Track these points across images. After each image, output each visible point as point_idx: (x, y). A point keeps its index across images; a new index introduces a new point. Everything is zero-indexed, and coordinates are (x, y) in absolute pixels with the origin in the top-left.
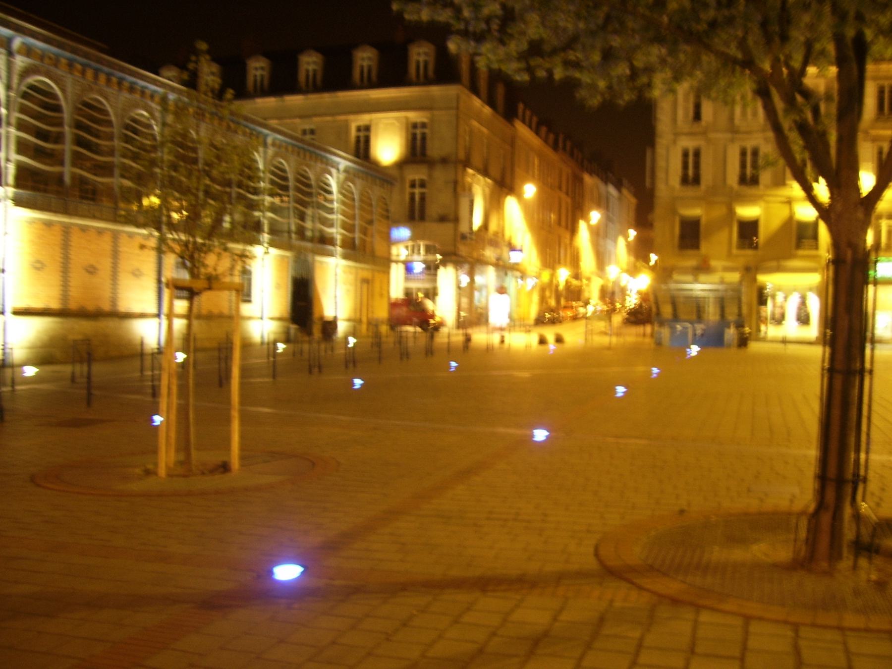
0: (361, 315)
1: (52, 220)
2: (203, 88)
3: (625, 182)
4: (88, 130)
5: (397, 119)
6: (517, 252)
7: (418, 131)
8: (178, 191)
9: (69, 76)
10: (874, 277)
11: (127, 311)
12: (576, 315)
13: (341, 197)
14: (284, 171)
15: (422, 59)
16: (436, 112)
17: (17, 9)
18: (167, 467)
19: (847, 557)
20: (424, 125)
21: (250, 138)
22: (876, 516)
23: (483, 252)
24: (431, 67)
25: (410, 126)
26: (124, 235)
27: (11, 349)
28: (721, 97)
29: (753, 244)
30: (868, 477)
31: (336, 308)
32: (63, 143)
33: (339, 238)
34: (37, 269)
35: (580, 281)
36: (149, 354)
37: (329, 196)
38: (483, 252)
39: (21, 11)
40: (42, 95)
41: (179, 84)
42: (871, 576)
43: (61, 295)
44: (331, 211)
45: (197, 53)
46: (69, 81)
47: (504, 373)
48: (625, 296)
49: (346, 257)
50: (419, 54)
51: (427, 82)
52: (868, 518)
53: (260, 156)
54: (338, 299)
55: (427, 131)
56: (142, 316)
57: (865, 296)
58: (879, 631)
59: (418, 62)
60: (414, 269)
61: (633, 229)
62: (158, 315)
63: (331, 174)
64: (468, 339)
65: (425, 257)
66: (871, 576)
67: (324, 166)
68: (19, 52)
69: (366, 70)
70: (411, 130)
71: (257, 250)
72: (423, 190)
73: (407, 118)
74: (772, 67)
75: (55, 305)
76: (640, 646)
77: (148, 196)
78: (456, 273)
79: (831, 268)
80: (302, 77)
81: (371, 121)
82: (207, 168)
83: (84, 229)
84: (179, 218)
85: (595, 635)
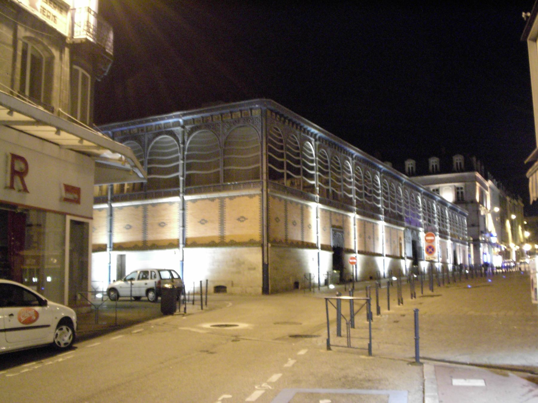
0: (123, 297)
2: (462, 237)
3: (519, 197)
4: (274, 152)
5: (450, 186)
6: (489, 225)
7: (460, 191)
8: (167, 110)
9: (302, 191)
11: (60, 319)
13: (404, 197)
14: (325, 157)
15: (410, 166)
16: (467, 183)
17: (43, 82)
19: (350, 292)
20: (462, 188)
22: (186, 242)
23: (155, 288)
24: (463, 164)
25: (456, 188)
27: (314, 291)
30: (412, 357)
31: (319, 272)
33: (449, 233)
34: (127, 229)
37: (349, 175)
38: (155, 288)
41: (70, 115)
42: (183, 162)
43: (255, 240)
44: (378, 195)
46: (329, 150)
47: (160, 145)
48: (329, 346)
49: (386, 220)
50: (457, 160)
51: (462, 171)
53: (378, 177)
54: (478, 361)
55: (463, 190)
56: (313, 246)
57: (22, 350)
58: (142, 287)
59: (457, 163)
60: (499, 266)
61: (492, 243)
63: (349, 161)
65: (373, 201)
66: (183, 162)
67: (345, 155)
68: (383, 173)
69: (435, 167)
70: (457, 191)
71: (379, 222)
73: (455, 186)
79: (51, 2)
80: (431, 168)
81: (439, 187)
83: (231, 198)
84: (382, 274)
85: (82, 296)
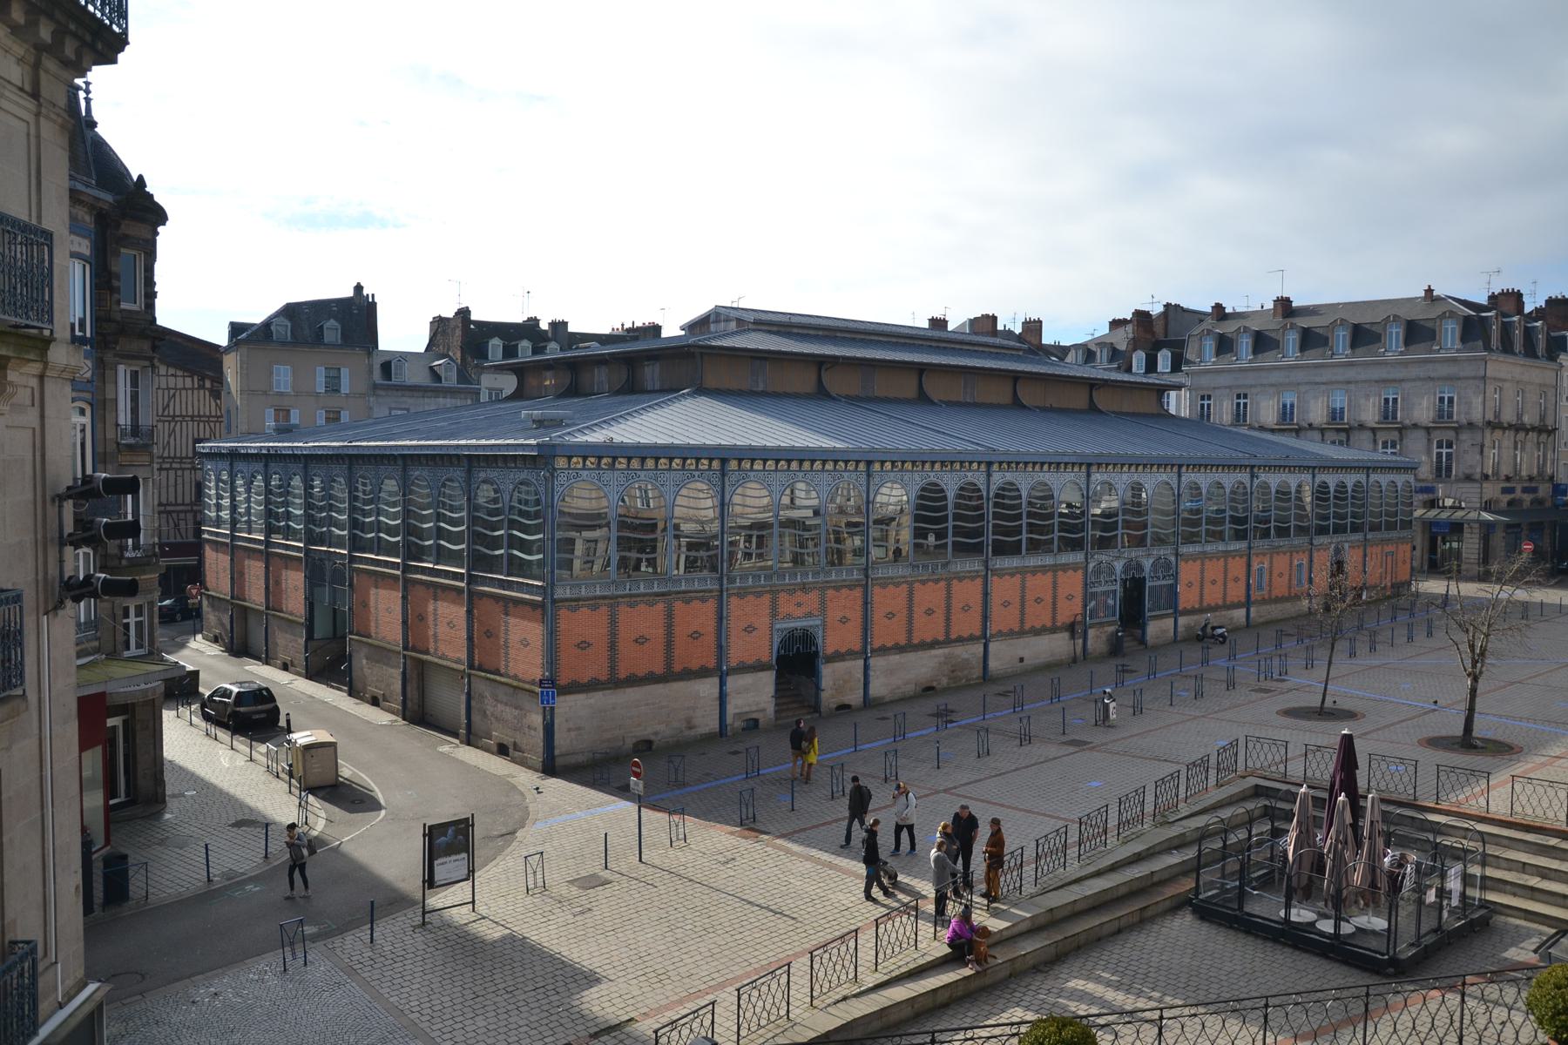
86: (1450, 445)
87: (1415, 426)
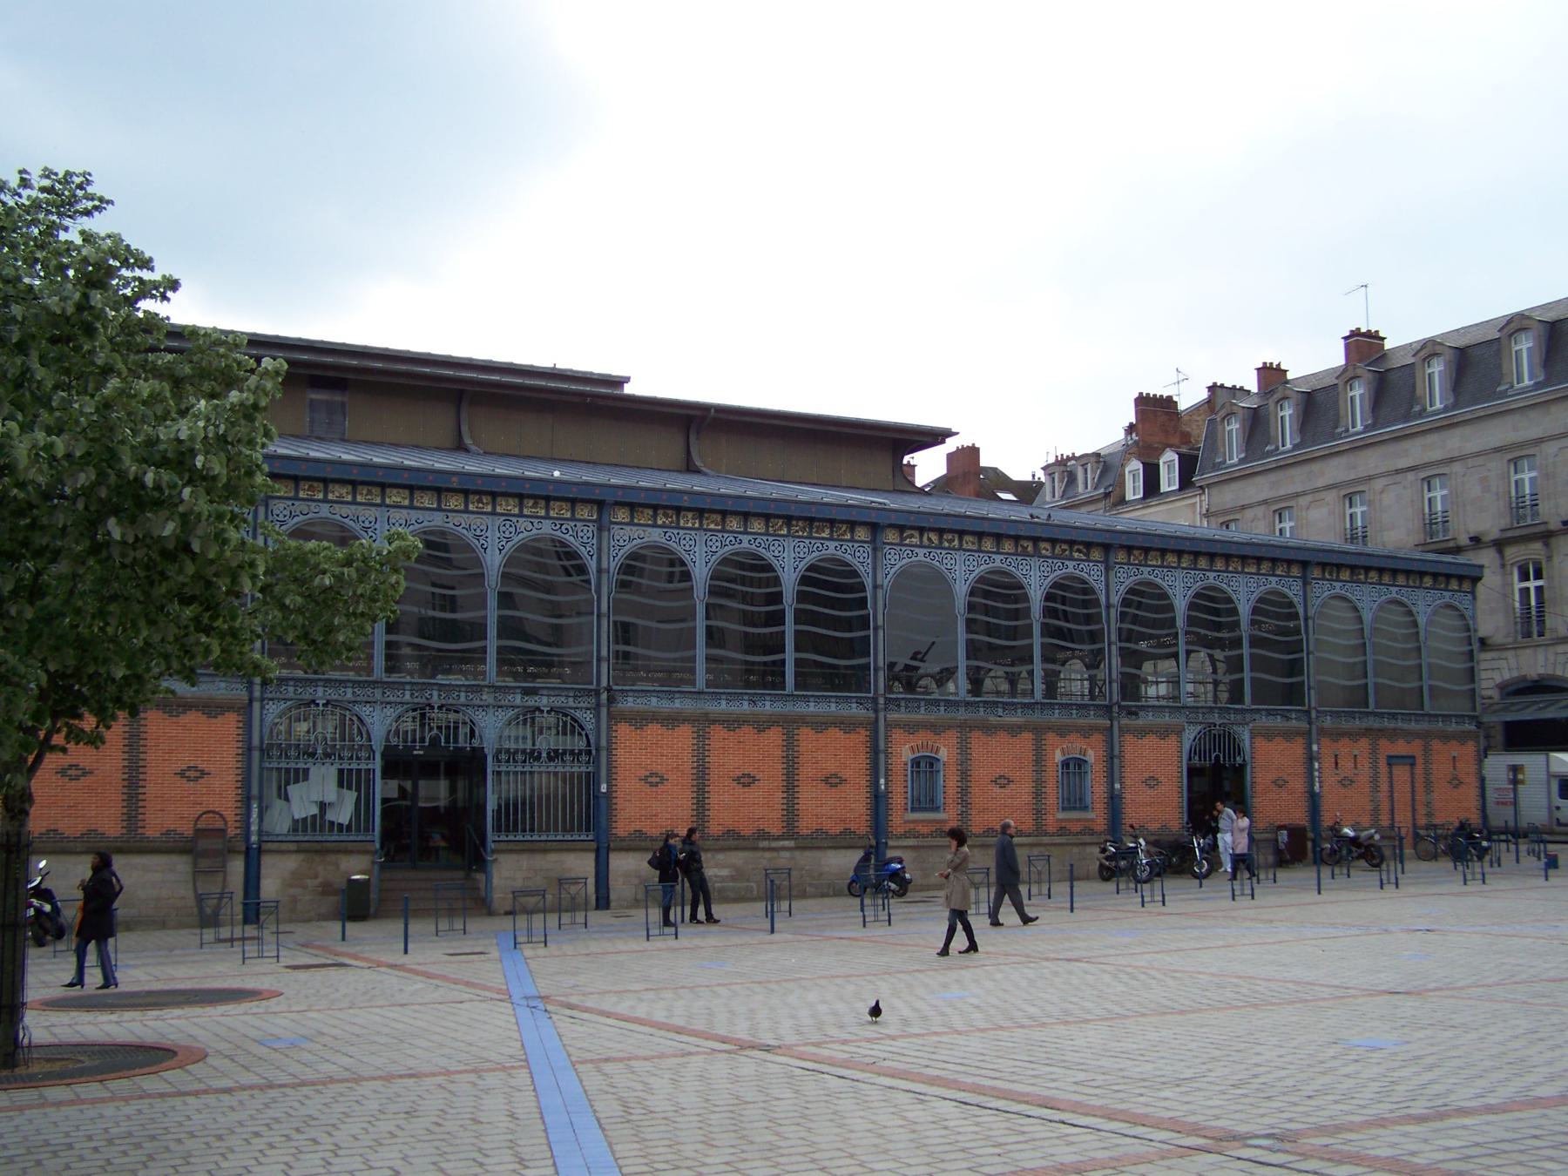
1: (1268, 423)
10: (23, 789)
12: (1556, 867)
18: (385, 801)
21: (167, 578)
26: (775, 831)
28: (163, 589)
29: (59, 419)
32: (1528, 589)
35: (1555, 768)
36: (1346, 376)
39: (1330, 679)
40: (536, 589)
45: (26, 938)
52: (451, 913)
62: (790, 831)
64: (28, 621)
72: (1540, 583)
74: (201, 548)
75: (1068, 883)
76: (71, 592)
77: (120, 523)
78: (499, 914)
82: (544, 755)
86: (1538, 576)
87: (1476, 541)
